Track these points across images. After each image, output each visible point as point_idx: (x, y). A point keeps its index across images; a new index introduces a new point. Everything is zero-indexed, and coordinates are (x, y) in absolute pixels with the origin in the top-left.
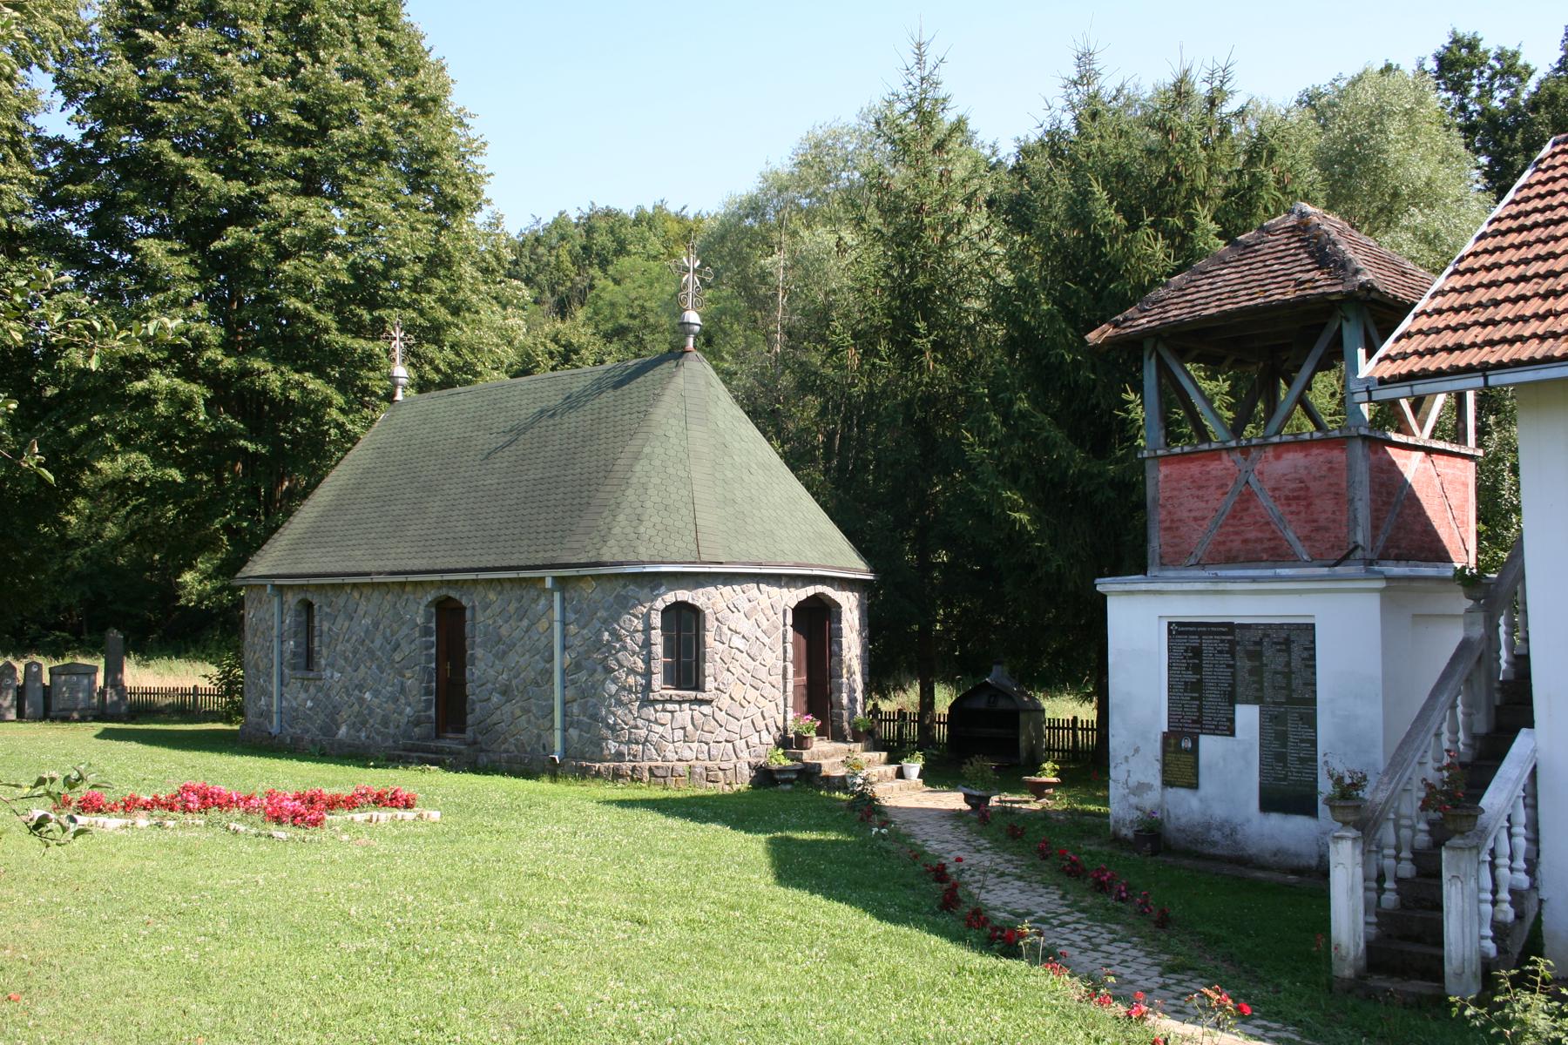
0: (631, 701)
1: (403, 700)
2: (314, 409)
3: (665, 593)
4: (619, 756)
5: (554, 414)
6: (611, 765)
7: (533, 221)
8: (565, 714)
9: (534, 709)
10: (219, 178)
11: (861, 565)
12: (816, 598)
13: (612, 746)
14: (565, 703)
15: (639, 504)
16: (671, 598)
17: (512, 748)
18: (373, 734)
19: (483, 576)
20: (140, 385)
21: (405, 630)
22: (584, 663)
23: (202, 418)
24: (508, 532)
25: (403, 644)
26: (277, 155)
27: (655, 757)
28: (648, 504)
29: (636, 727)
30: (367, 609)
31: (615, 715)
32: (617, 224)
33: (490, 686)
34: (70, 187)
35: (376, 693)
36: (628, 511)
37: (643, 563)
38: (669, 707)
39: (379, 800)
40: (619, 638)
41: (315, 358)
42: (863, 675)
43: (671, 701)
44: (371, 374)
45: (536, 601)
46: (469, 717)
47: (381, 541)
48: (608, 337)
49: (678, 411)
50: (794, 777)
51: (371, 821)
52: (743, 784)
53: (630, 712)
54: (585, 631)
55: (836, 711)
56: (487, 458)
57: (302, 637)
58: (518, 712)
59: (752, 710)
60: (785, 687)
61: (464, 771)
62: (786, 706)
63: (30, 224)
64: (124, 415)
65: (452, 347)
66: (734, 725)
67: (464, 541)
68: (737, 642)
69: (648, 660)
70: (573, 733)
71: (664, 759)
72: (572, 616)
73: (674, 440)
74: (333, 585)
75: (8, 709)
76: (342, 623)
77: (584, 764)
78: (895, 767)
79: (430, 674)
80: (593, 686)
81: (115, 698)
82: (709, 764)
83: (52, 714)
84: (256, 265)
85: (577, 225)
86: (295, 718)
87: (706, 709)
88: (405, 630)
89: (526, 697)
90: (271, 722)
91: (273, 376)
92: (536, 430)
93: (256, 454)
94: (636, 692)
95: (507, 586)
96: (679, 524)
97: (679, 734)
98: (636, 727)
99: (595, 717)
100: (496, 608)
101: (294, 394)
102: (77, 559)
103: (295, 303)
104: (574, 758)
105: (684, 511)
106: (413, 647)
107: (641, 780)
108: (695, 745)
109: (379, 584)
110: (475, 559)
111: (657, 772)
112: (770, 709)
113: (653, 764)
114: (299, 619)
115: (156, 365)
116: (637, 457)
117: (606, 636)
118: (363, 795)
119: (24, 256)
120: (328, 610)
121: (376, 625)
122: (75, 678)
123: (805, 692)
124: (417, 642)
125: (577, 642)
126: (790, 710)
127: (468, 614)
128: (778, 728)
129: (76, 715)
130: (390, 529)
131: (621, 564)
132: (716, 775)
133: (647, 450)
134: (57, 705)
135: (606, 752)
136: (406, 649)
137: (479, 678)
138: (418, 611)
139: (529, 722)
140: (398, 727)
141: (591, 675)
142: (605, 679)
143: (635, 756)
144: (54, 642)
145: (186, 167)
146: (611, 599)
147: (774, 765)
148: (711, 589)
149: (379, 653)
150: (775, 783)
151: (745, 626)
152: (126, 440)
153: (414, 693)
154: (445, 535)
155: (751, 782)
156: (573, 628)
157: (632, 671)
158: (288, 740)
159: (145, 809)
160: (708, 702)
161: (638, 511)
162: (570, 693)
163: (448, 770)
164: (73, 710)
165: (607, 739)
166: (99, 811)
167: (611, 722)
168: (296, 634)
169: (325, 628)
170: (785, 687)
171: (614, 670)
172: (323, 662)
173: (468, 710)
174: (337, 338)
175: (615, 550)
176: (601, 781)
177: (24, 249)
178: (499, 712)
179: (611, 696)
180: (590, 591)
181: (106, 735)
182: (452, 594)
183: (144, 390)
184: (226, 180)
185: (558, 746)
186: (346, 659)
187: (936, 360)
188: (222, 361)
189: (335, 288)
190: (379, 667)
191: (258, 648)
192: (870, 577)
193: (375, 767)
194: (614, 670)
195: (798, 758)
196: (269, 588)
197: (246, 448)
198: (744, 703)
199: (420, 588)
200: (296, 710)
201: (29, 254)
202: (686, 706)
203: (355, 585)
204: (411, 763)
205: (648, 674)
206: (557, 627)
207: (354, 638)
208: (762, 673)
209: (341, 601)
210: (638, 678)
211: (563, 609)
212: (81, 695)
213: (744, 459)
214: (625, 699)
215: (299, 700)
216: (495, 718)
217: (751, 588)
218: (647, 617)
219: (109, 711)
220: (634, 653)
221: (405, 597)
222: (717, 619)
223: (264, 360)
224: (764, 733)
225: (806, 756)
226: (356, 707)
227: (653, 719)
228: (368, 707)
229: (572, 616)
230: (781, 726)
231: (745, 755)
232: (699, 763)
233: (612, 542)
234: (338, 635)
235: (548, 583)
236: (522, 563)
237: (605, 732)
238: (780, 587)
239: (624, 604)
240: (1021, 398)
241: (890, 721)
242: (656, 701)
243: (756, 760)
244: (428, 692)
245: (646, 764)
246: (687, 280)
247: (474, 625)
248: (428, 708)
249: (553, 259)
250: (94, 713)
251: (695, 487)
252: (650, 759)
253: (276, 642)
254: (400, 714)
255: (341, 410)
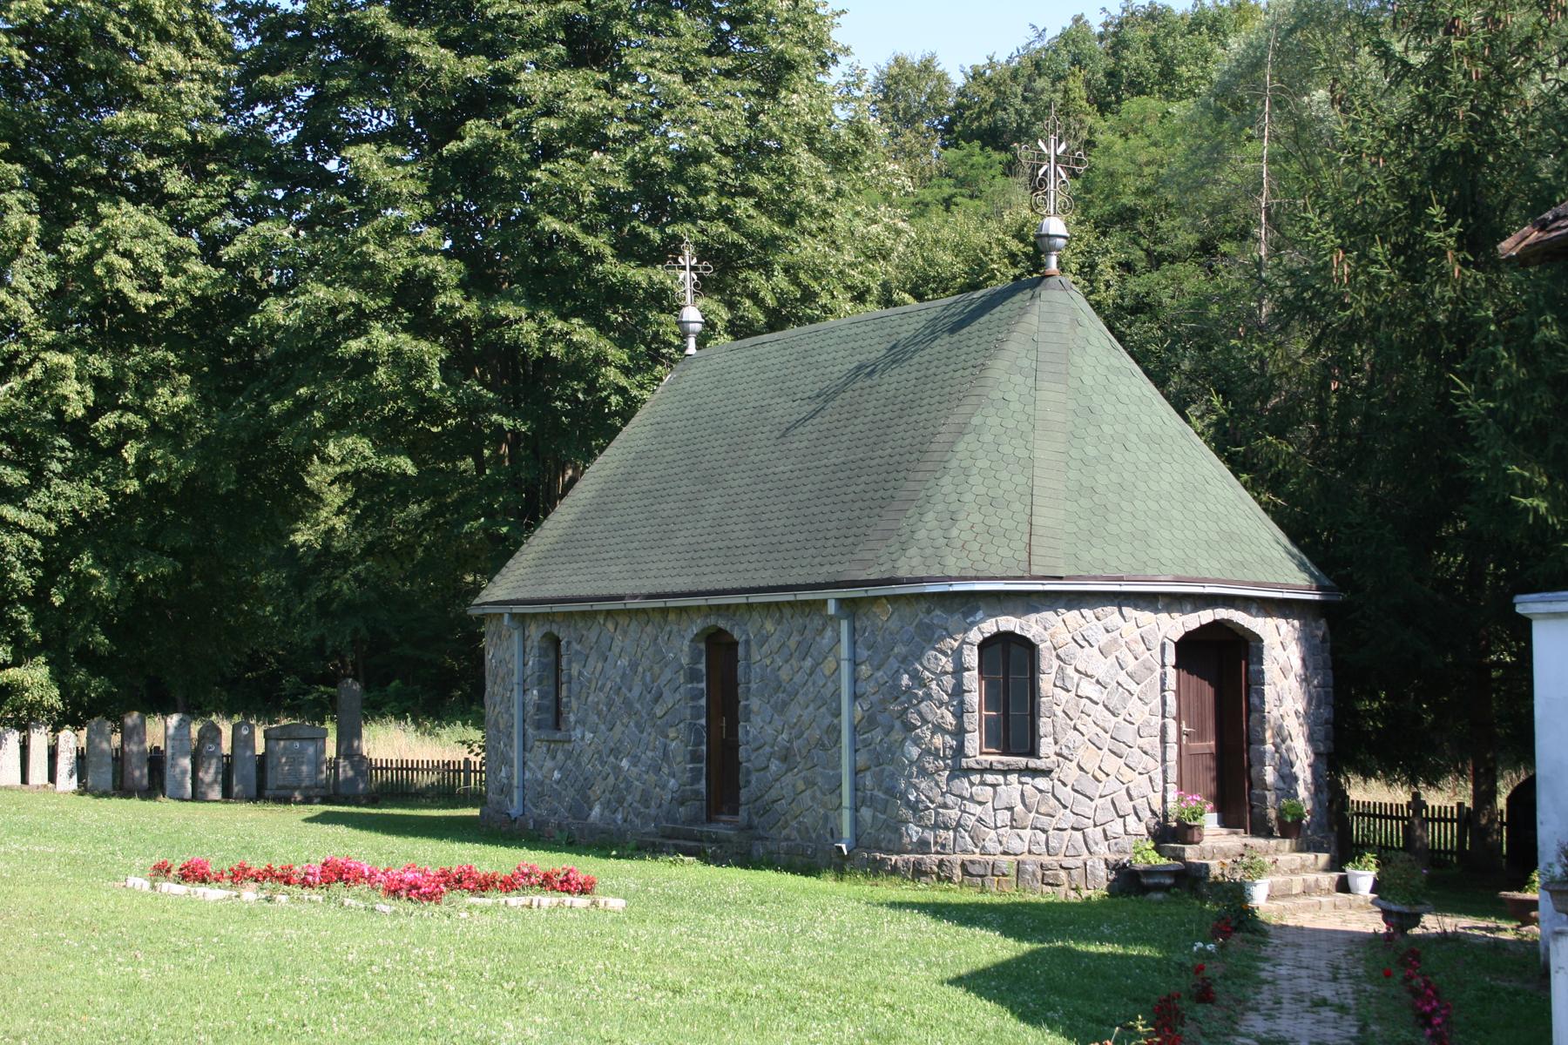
0: (938, 770)
1: (665, 770)
2: (583, 368)
3: (983, 620)
4: (923, 846)
5: (873, 371)
6: (912, 857)
7: (1032, 35)
8: (856, 788)
9: (819, 780)
10: (450, 55)
11: (1302, 579)
12: (1217, 624)
13: (914, 832)
14: (856, 772)
15: (954, 497)
16: (990, 627)
17: (794, 834)
18: (631, 816)
19: (755, 599)
20: (355, 345)
21: (668, 674)
22: (879, 718)
23: (436, 386)
24: (792, 538)
25: (666, 692)
26: (529, 14)
27: (971, 847)
28: (968, 497)
29: (945, 806)
30: (625, 643)
31: (917, 789)
32: (1162, 32)
33: (767, 749)
34: (267, 78)
35: (635, 761)
36: (940, 507)
37: (950, 578)
38: (989, 778)
39: (547, 882)
40: (922, 684)
41: (587, 296)
42: (1311, 739)
43: (991, 770)
44: (663, 317)
45: (821, 632)
46: (742, 791)
47: (642, 553)
48: (1103, 227)
49: (1026, 363)
50: (1168, 881)
51: (530, 907)
52: (1097, 888)
53: (937, 784)
54: (880, 673)
55: (1257, 791)
56: (783, 435)
57: (549, 685)
58: (801, 786)
59: (1111, 785)
60: (1164, 753)
61: (729, 865)
62: (1165, 781)
63: (219, 131)
64: (337, 386)
65: (786, 271)
66: (1085, 807)
67: (739, 552)
68: (1088, 688)
69: (959, 714)
70: (866, 813)
71: (984, 851)
72: (863, 653)
73: (1015, 406)
74: (583, 613)
75: (210, 785)
76: (594, 664)
77: (878, 856)
78: (1335, 875)
79: (698, 733)
80: (889, 749)
81: (350, 773)
82: (1046, 859)
83: (267, 793)
84: (502, 171)
85: (1101, 37)
86: (540, 795)
87: (1042, 783)
88: (668, 674)
89: (809, 765)
90: (512, 801)
91: (528, 326)
92: (850, 393)
93: (514, 432)
94: (945, 758)
95: (787, 612)
96: (1006, 524)
97: (1004, 816)
98: (945, 806)
99: (891, 792)
100: (774, 643)
101: (557, 350)
102: (347, 581)
103: (551, 223)
104: (868, 849)
105: (1017, 506)
106: (678, 696)
107: (950, 879)
108: (1027, 833)
109: (637, 610)
110: (749, 575)
111: (972, 869)
112: (1140, 784)
113: (967, 857)
114: (545, 660)
115: (376, 315)
116: (961, 432)
117: (905, 680)
118: (528, 875)
119: (213, 174)
120: (578, 647)
121: (634, 666)
122: (297, 744)
123: (1212, 764)
124: (682, 690)
125: (870, 688)
126: (1172, 788)
127: (741, 650)
128: (1153, 813)
129: (298, 796)
130: (656, 536)
131: (920, 580)
132: (1057, 878)
133: (975, 421)
134: (274, 781)
135: (906, 840)
136: (669, 699)
137: (755, 738)
138: (682, 647)
139: (813, 798)
140: (660, 806)
141: (887, 734)
142: (905, 739)
143: (943, 846)
144: (318, 702)
145: (408, 42)
146: (912, 629)
147: (1140, 864)
148: (1049, 615)
149: (638, 706)
150: (1147, 889)
151: (1101, 667)
152: (339, 423)
153: (679, 759)
154: (720, 544)
155: (1109, 888)
156: (865, 670)
157: (938, 728)
158: (531, 826)
159: (256, 881)
160: (1047, 773)
161: (952, 508)
162: (862, 759)
163: (707, 863)
164: (296, 788)
165: (907, 822)
166: (204, 881)
167: (912, 798)
168: (540, 681)
169: (575, 672)
170: (1164, 753)
171: (916, 727)
172: (572, 718)
173: (742, 783)
174: (614, 269)
175: (916, 561)
176: (897, 880)
177: (211, 167)
178: (778, 785)
179: (912, 763)
180: (885, 618)
181: (325, 819)
182: (722, 624)
183: (360, 351)
184: (460, 57)
185: (846, 832)
186: (599, 714)
187: (1465, 263)
188: (461, 307)
189: (608, 201)
190: (637, 725)
191: (498, 699)
192: (1314, 596)
193: (618, 857)
194: (916, 727)
195: (1179, 857)
196: (506, 616)
197: (501, 425)
198: (1101, 776)
199: (685, 616)
200: (542, 784)
201: (220, 172)
202: (1013, 778)
203: (609, 613)
204: (661, 852)
205: (960, 732)
206: (845, 668)
207: (609, 685)
208: (1128, 734)
209: (593, 636)
210: (948, 738)
211: (853, 643)
212: (304, 768)
213: (1118, 427)
214: (930, 767)
215: (545, 769)
216: (773, 794)
217: (1111, 614)
218: (958, 654)
219: (342, 790)
220: (941, 703)
221: (668, 628)
222: (1058, 657)
223: (516, 304)
224: (1131, 819)
225: (1191, 853)
226: (611, 779)
227: (968, 796)
228: (625, 778)
229: (863, 653)
230: (1159, 811)
231: (1102, 849)
232: (1033, 857)
233: (912, 551)
234: (590, 681)
235: (831, 608)
236: (801, 581)
237: (905, 812)
238: (1156, 611)
239: (929, 636)
240: (1545, 323)
241: (1386, 817)
242: (970, 770)
243: (1117, 857)
244: (695, 757)
245: (958, 858)
246: (1045, 174)
247: (748, 666)
248: (695, 780)
249: (1058, 97)
250: (323, 792)
251: (1037, 471)
252: (965, 851)
253: (516, 695)
254: (663, 787)
255: (626, 371)
